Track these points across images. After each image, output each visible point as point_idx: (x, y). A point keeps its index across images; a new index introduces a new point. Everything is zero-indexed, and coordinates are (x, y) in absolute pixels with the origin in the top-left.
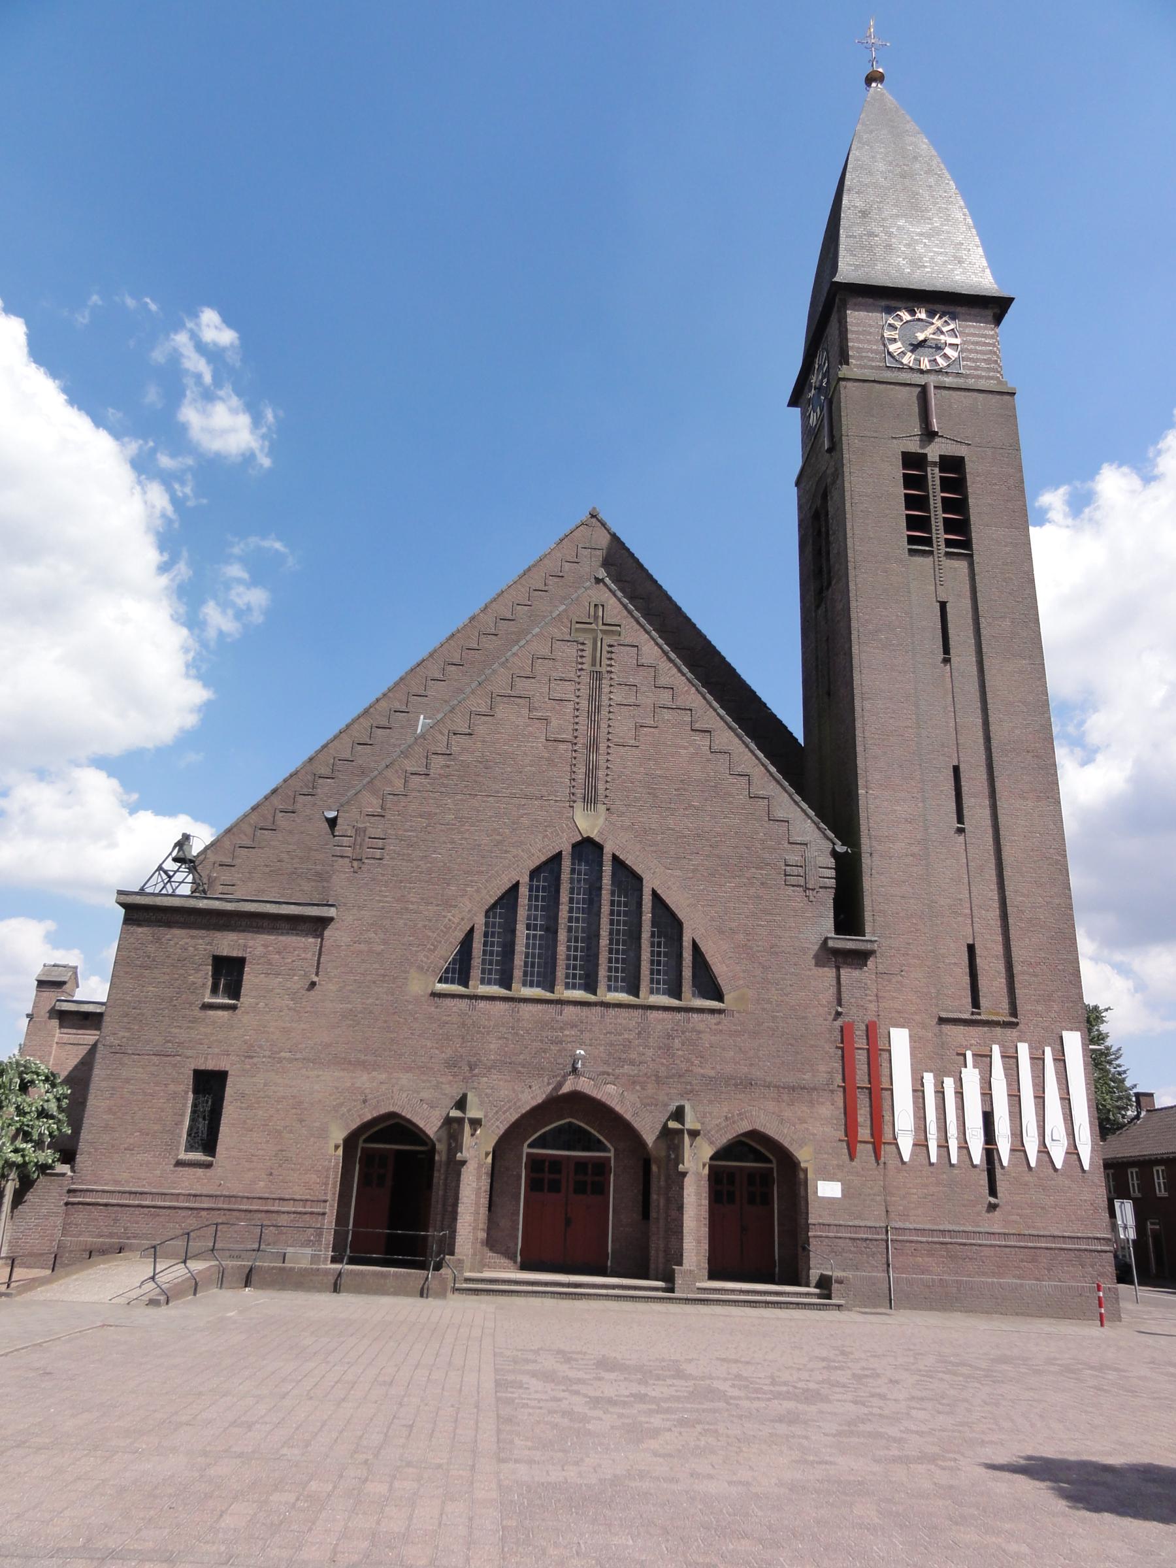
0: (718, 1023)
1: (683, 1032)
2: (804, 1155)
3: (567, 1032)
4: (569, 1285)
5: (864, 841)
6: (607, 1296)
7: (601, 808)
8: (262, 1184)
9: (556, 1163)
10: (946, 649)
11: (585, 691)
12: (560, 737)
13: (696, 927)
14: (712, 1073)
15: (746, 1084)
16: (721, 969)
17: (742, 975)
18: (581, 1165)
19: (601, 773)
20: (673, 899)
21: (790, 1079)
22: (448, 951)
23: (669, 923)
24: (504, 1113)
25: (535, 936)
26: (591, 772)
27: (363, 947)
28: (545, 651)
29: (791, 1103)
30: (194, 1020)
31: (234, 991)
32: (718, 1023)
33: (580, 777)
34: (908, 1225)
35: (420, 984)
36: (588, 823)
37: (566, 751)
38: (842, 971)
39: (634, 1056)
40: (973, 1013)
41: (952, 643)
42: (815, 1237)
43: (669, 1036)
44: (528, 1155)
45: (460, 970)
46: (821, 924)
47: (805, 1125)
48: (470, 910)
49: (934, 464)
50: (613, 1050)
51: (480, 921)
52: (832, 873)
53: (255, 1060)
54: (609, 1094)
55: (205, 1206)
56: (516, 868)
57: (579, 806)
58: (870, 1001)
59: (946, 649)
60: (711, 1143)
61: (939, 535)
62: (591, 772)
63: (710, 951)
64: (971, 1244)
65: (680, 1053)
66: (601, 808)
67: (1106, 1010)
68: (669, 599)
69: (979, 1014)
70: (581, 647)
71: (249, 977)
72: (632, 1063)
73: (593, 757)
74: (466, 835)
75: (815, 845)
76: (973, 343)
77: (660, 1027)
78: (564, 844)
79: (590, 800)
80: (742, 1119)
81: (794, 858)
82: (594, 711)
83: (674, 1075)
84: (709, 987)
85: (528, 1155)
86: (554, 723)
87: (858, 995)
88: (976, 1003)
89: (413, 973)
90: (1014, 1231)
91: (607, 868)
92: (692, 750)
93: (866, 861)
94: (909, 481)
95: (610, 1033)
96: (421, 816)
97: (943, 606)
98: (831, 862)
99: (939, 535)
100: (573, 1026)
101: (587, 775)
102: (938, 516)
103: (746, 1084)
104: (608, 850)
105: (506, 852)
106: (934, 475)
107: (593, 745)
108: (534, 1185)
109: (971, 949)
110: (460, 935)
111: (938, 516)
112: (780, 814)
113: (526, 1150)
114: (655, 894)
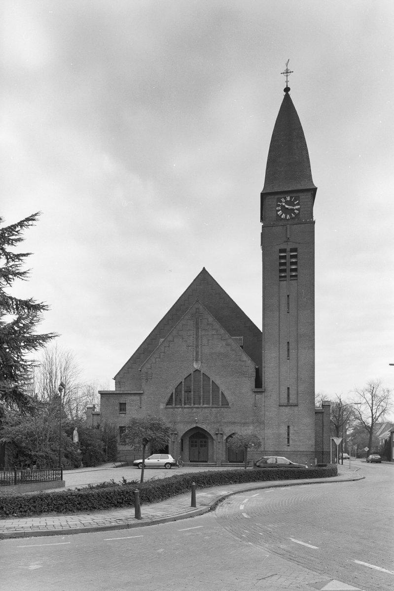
19: (199, 353)
21: (243, 421)
28: (157, 359)
29: (243, 427)
30: (118, 417)
31: (125, 410)
33: (195, 354)
35: (162, 406)
36: (196, 366)
38: (145, 470)
45: (170, 402)
46: (251, 383)
48: (171, 389)
50: (202, 417)
54: (204, 427)
56: (181, 379)
57: (195, 362)
63: (226, 393)
67: (391, 365)
68: (226, 293)
71: (128, 407)
73: (288, 250)
75: (250, 365)
82: (197, 339)
84: (225, 404)
88: (288, 401)
104: (202, 372)
107: (197, 346)
110: (170, 395)
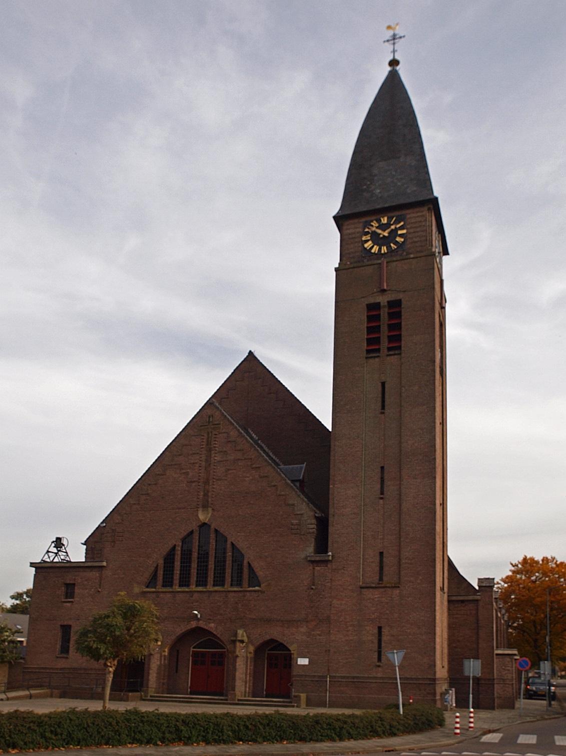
0: (258, 596)
1: (243, 601)
2: (293, 648)
3: (194, 604)
4: (189, 698)
5: (331, 511)
6: (197, 702)
7: (210, 509)
8: (84, 664)
9: (203, 654)
10: (383, 407)
11: (204, 458)
12: (193, 480)
13: (249, 555)
14: (254, 617)
15: (269, 621)
16: (260, 574)
17: (269, 575)
18: (214, 654)
20: (242, 545)
22: (147, 575)
23: (238, 556)
24: (170, 636)
25: (187, 566)
26: (206, 495)
27: (116, 576)
32: (258, 596)
34: (337, 675)
37: (195, 486)
39: (222, 612)
40: (380, 584)
41: (386, 403)
42: (295, 680)
43: (236, 603)
44: (193, 651)
45: (152, 582)
47: (294, 636)
49: (384, 306)
51: (161, 562)
52: (314, 526)
53: (80, 621)
55: (66, 672)
56: (174, 540)
58: (328, 582)
59: (383, 407)
60: (253, 645)
61: (384, 344)
62: (206, 495)
63: (255, 565)
64: (366, 682)
65: (241, 610)
66: (210, 509)
69: (382, 584)
70: (202, 437)
71: (77, 591)
72: (221, 614)
74: (155, 528)
75: (306, 513)
76: (418, 232)
77: (232, 600)
78: (194, 526)
79: (205, 507)
80: (266, 635)
81: (295, 522)
83: (238, 619)
84: (254, 580)
85: (193, 651)
86: (191, 474)
87: (322, 580)
88: (381, 579)
89: (135, 585)
90: (387, 676)
91: (213, 536)
92: (251, 478)
93: (331, 519)
94: (370, 319)
95: (212, 603)
96: (137, 522)
97: (383, 384)
98: (314, 521)
99: (384, 344)
100: (197, 602)
101: (204, 495)
102: (384, 332)
103: (269, 621)
104: (212, 527)
105: (170, 533)
106: (384, 313)
108: (194, 663)
109: (381, 554)
111: (384, 332)
112: (291, 502)
113: (192, 649)
114: (232, 544)
